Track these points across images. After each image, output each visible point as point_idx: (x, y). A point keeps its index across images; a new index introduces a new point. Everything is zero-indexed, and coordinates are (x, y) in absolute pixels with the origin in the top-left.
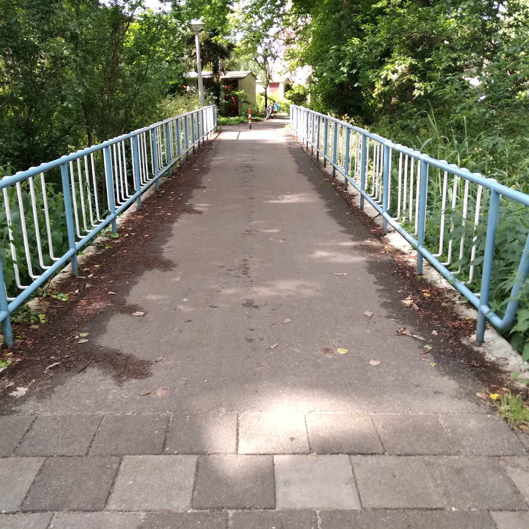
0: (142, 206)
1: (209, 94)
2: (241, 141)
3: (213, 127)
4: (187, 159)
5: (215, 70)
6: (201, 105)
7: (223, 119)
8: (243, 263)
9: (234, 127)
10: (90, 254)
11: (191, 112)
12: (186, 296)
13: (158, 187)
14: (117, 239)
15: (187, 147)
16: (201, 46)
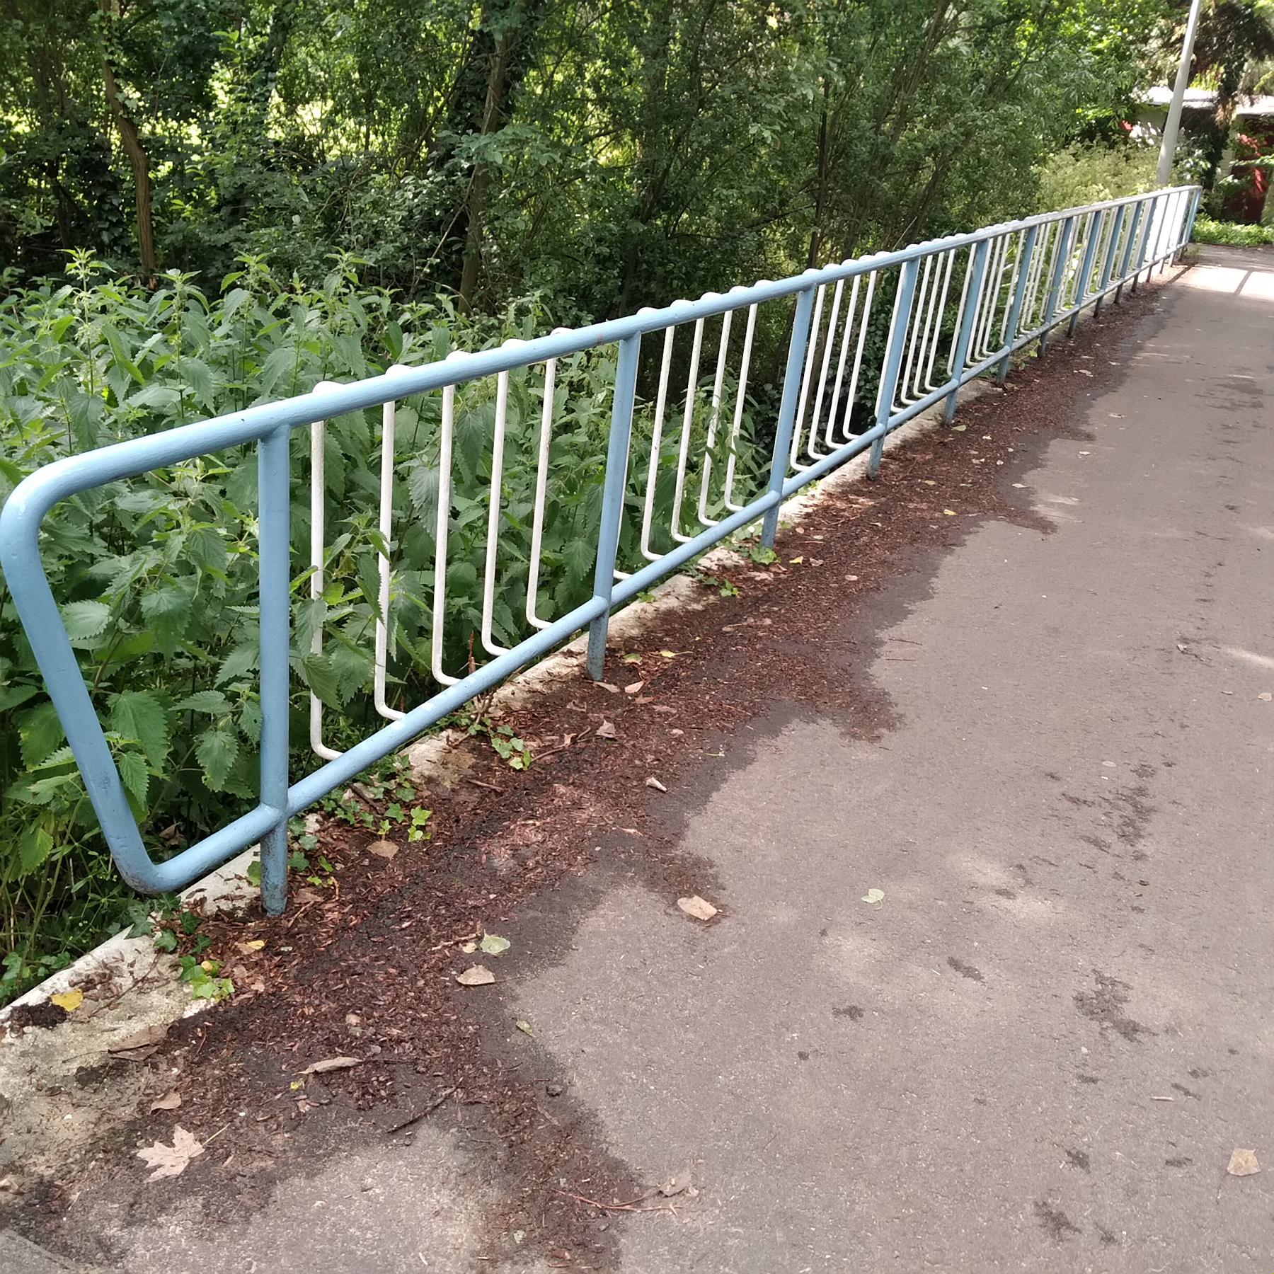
0: (884, 466)
1: (1190, 154)
2: (1248, 300)
3: (1173, 248)
4: (1068, 335)
5: (1227, 91)
6: (1158, 181)
7: (1212, 226)
8: (1133, 782)
9: (1238, 255)
10: (672, 603)
11: (1120, 201)
12: (885, 872)
13: (951, 413)
14: (766, 568)
15: (1078, 301)
16: (1203, 17)
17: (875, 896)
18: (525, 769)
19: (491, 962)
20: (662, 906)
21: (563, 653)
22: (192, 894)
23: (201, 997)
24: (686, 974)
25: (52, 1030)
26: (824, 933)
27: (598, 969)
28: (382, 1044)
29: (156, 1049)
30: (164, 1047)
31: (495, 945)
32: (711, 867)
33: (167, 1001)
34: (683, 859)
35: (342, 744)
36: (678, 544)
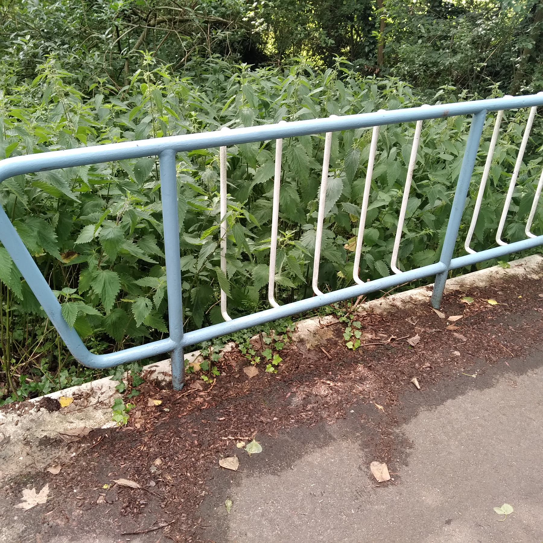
17: (507, 509)
18: (354, 349)
19: (243, 456)
20: (360, 461)
21: (428, 288)
22: (152, 367)
23: (115, 421)
24: (341, 512)
25: (50, 413)
26: (448, 522)
27: (295, 487)
28: (157, 483)
29: (78, 439)
30: (83, 439)
31: (255, 448)
32: (411, 448)
33: (102, 417)
34: (398, 436)
35: (234, 315)
36: (527, 238)
